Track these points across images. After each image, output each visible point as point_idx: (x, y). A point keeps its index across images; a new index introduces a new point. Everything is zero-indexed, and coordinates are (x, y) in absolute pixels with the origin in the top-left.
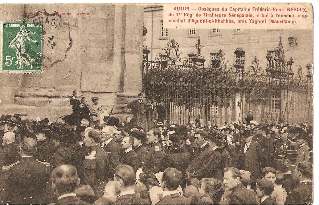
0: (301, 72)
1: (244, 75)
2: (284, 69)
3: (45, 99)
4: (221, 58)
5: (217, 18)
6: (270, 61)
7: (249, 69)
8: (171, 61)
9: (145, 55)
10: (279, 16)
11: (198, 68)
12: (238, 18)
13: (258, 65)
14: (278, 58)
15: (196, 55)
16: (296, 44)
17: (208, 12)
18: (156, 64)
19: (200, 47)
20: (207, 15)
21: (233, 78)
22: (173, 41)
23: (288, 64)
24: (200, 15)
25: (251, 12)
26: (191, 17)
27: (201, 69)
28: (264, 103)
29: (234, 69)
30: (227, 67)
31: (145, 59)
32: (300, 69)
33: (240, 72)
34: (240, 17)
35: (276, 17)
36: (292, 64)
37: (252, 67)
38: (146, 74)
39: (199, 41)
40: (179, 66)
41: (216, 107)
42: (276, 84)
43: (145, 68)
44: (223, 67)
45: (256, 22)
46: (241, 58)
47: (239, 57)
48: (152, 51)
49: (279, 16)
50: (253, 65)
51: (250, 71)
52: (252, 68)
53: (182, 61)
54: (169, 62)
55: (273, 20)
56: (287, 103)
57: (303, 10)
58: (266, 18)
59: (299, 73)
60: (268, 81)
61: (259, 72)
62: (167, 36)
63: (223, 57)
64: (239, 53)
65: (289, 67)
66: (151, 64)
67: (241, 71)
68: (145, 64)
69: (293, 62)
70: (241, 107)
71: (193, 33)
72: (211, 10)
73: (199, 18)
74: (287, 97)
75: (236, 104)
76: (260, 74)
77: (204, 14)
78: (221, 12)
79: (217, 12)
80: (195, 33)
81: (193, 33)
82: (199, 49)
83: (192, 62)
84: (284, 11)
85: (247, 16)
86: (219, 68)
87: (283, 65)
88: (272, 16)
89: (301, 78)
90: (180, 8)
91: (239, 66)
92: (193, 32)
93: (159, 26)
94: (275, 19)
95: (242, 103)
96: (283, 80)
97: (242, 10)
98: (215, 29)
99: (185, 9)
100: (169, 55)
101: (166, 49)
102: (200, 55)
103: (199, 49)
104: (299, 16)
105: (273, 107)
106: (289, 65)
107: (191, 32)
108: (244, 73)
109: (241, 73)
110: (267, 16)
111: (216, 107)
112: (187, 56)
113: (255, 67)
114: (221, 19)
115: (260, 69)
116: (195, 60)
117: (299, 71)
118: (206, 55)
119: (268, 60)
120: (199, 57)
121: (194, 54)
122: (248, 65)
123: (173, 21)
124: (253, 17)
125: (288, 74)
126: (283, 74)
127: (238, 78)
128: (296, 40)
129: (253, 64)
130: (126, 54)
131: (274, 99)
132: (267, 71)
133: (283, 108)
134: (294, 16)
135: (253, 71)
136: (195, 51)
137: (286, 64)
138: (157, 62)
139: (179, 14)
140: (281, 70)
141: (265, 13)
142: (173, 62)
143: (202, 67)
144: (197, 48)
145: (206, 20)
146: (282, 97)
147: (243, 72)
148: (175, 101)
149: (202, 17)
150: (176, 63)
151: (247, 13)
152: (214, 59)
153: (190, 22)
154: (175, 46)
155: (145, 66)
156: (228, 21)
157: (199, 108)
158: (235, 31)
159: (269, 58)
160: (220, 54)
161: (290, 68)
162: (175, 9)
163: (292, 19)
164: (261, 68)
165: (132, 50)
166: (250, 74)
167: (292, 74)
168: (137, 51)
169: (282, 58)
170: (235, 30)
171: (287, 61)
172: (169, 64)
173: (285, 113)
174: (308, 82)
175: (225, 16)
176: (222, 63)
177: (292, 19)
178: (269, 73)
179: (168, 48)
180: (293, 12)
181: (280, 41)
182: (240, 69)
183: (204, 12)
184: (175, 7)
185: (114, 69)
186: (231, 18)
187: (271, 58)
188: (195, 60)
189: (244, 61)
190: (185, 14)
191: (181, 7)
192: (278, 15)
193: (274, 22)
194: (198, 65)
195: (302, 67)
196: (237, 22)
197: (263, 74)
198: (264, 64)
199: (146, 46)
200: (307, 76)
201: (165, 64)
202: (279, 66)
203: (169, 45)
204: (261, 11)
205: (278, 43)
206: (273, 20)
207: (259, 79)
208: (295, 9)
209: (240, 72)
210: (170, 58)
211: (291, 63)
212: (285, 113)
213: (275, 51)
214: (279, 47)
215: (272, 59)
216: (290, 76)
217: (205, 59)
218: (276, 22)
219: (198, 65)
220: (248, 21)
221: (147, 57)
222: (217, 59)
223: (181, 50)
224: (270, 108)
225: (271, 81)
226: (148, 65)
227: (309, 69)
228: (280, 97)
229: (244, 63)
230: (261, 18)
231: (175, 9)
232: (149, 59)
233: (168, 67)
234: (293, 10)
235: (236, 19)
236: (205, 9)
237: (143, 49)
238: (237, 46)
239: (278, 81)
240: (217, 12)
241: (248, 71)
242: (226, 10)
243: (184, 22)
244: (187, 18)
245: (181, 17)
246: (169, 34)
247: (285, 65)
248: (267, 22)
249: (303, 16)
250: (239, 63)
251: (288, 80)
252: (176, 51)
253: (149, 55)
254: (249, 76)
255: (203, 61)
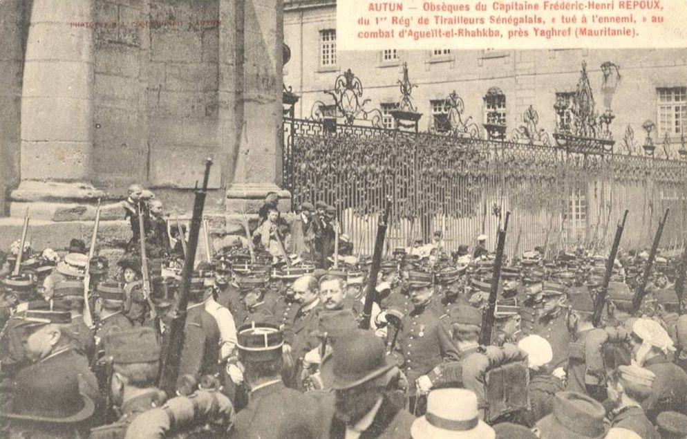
0: (632, 139)
1: (506, 147)
2: (594, 131)
3: (74, 205)
4: (454, 110)
5: (463, 26)
6: (562, 114)
7: (518, 133)
8: (345, 118)
9: (287, 107)
10: (600, 20)
11: (404, 132)
12: (512, 27)
13: (535, 124)
14: (578, 107)
15: (398, 104)
16: (619, 76)
17: (446, 14)
18: (311, 125)
19: (408, 87)
20: (444, 21)
21: (481, 154)
22: (349, 75)
23: (601, 122)
24: (426, 21)
25: (540, 13)
26: (408, 24)
27: (411, 133)
28: (551, 209)
29: (483, 134)
30: (470, 129)
31: (288, 115)
32: (630, 131)
33: (497, 140)
34: (516, 24)
35: (594, 21)
36: (610, 122)
37: (523, 129)
38: (290, 147)
39: (406, 71)
40: (364, 130)
41: (446, 216)
42: (575, 165)
43: (287, 134)
44: (459, 128)
45: (417, 36)
46: (500, 110)
47: (494, 107)
48: (301, 97)
49: (600, 20)
50: (525, 125)
51: (519, 137)
52: (522, 131)
53: (370, 117)
54: (341, 121)
55: (585, 29)
56: (602, 206)
57: (654, 5)
58: (571, 25)
59: (626, 142)
60: (560, 158)
61: (538, 139)
62: (334, 64)
63: (459, 108)
64: (495, 99)
65: (604, 128)
66: (301, 125)
67: (499, 137)
68: (287, 126)
69: (613, 117)
70: (500, 216)
71: (392, 57)
72: (451, 8)
73: (423, 28)
74: (602, 193)
75: (490, 210)
76: (542, 144)
77: (437, 19)
78: (473, 14)
79: (464, 14)
80: (395, 57)
81: (392, 57)
82: (406, 94)
83: (390, 120)
84: (613, 8)
85: (531, 21)
86: (449, 132)
87: (591, 123)
88: (584, 20)
89: (630, 153)
90: (383, 7)
91: (496, 128)
92: (392, 54)
93: (318, 42)
94: (590, 25)
95: (503, 209)
96: (592, 156)
97: (521, 8)
98: (390, 51)
99: (392, 8)
100: (340, 105)
101: (334, 92)
102: (408, 103)
103: (406, 94)
104: (644, 19)
105: (571, 217)
106: (604, 124)
107: (326, 60)
108: (506, 142)
109: (499, 142)
110: (574, 20)
111: (446, 216)
112: (379, 107)
113: (529, 128)
114: (471, 28)
115: (542, 133)
116: (399, 115)
117: (626, 137)
118: (420, 103)
119: (559, 113)
120: (406, 109)
121: (396, 101)
122: (514, 122)
123: (367, 35)
124: (544, 22)
125: (603, 142)
126: (590, 143)
127: (493, 153)
128: (618, 68)
129: (525, 121)
130: (246, 104)
131: (573, 198)
132: (556, 136)
133: (593, 220)
134: (633, 19)
135: (525, 136)
136: (396, 95)
137: (598, 121)
138: (315, 122)
139: (381, 19)
140: (586, 134)
141: (569, 14)
142: (351, 119)
143: (412, 130)
144: (403, 88)
145: (440, 31)
146: (591, 191)
147: (505, 140)
148: (355, 206)
149: (432, 25)
150: (356, 123)
151: (530, 13)
152: (440, 112)
153: (403, 36)
154: (353, 84)
155: (289, 129)
156: (488, 33)
157: (409, 219)
158: (431, 55)
159: (560, 110)
160: (452, 102)
161: (608, 131)
162: (371, 7)
163: (628, 26)
164: (543, 130)
165: (259, 96)
166: (535, 146)
167: (612, 143)
168: (271, 98)
169: (588, 109)
170: (430, 52)
171: (601, 114)
172: (341, 125)
173: (597, 228)
174: (648, 160)
175: (482, 21)
176: (457, 119)
177: (628, 26)
178: (562, 142)
179: (337, 90)
180: (632, 11)
181: (584, 70)
182: (497, 134)
183: (436, 13)
184: (371, 5)
185: (219, 139)
186: (494, 27)
187: (564, 108)
188: (399, 115)
189: (504, 115)
190: (394, 20)
191: (385, 4)
192: (599, 17)
193: (587, 32)
194: (405, 126)
195: (633, 127)
196: (506, 35)
197: (547, 143)
198: (548, 121)
199: (290, 87)
200: (646, 147)
201: (330, 125)
202: (583, 125)
203: (341, 83)
204: (507, 5)
205: (579, 75)
206: (585, 29)
207: (542, 155)
208: (636, 3)
209: (497, 140)
210: (344, 112)
211: (608, 119)
212: (597, 228)
213: (573, 94)
214: (582, 83)
215: (566, 110)
216: (607, 147)
217: (419, 112)
218: (591, 33)
219: (405, 126)
220: (532, 32)
221: (292, 111)
222: (445, 113)
223: (366, 94)
224: (565, 217)
225: (565, 158)
226: (296, 126)
227: (649, 132)
228: (585, 192)
229: (504, 120)
230: (559, 26)
231: (371, 7)
232: (297, 116)
233: (339, 131)
234: (632, 6)
235: (504, 28)
236: (438, 6)
237: (284, 93)
238: (489, 84)
239: (580, 160)
240: (464, 14)
241: (515, 136)
242: (485, 9)
243: (393, 36)
244: (398, 28)
245: (386, 26)
246: (337, 59)
247: (595, 124)
248: (573, 33)
249: (654, 19)
250: (493, 120)
251: (602, 156)
252: (356, 96)
253: (297, 106)
254: (518, 148)
255: (417, 117)
